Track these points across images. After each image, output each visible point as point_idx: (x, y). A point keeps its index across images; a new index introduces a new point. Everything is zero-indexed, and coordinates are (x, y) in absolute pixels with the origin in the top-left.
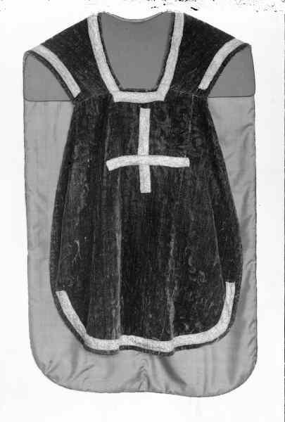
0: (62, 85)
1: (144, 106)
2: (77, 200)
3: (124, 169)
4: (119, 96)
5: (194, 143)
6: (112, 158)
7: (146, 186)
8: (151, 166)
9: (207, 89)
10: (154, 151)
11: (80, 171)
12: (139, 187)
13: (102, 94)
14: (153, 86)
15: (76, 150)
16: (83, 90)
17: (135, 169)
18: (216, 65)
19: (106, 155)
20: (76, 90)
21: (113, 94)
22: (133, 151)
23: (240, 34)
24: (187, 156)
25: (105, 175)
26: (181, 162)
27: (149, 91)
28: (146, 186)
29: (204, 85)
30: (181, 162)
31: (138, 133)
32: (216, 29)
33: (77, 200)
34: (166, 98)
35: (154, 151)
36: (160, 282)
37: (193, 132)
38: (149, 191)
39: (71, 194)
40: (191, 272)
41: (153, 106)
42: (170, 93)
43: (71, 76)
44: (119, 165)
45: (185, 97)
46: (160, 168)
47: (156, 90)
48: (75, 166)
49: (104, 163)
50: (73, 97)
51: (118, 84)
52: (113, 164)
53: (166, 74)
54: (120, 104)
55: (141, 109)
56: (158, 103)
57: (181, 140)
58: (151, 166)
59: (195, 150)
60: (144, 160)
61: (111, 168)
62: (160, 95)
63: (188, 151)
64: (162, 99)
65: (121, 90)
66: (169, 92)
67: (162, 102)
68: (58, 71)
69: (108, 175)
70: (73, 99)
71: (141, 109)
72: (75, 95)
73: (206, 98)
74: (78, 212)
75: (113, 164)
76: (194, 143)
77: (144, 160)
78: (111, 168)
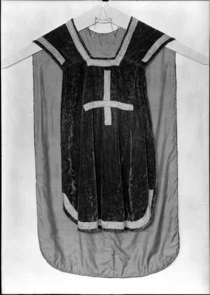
0: (67, 215)
1: (107, 68)
3: (94, 110)
4: (90, 63)
5: (136, 95)
6: (87, 102)
7: (108, 121)
8: (112, 108)
9: (147, 62)
12: (104, 121)
13: (79, 61)
14: (114, 56)
16: (67, 60)
17: (101, 110)
19: (83, 101)
20: (62, 60)
21: (86, 60)
22: (100, 98)
23: (168, 32)
25: (83, 114)
27: (110, 59)
28: (108, 121)
30: (128, 107)
31: (103, 86)
34: (120, 65)
36: (109, 196)
37: (136, 88)
42: (123, 61)
43: (57, 51)
44: (91, 107)
45: (132, 64)
47: (114, 58)
49: (82, 106)
50: (60, 64)
51: (89, 54)
52: (87, 107)
53: (122, 48)
54: (91, 67)
55: (105, 71)
56: (115, 67)
58: (112, 108)
60: (107, 104)
61: (86, 109)
62: (117, 62)
64: (118, 65)
65: (92, 58)
66: (123, 60)
67: (118, 66)
68: (49, 50)
69: (85, 115)
70: (61, 66)
71: (105, 71)
72: (62, 63)
73: (145, 68)
74: (69, 139)
75: (87, 107)
76: (136, 95)
77: (107, 104)
78: (86, 109)
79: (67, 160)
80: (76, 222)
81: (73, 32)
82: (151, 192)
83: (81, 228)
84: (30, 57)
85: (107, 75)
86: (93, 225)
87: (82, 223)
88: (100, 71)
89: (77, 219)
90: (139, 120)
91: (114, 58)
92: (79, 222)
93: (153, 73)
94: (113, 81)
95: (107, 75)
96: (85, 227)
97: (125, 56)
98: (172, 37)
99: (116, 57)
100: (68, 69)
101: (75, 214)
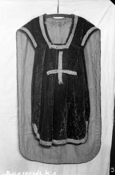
2: (39, 87)
7: (60, 80)
10: (64, 68)
11: (40, 76)
15: (37, 68)
18: (60, 78)
20: (36, 45)
23: (97, 25)
24: (76, 71)
26: (74, 73)
28: (60, 80)
29: (83, 44)
32: (88, 22)
33: (39, 87)
34: (69, 48)
35: (64, 68)
38: (76, 74)
39: (37, 86)
40: (76, 116)
41: (64, 50)
42: (71, 46)
46: (66, 74)
48: (37, 75)
52: (49, 73)
55: (60, 52)
56: (66, 49)
57: (74, 65)
59: (79, 69)
62: (67, 46)
63: (76, 69)
64: (68, 48)
65: (52, 44)
70: (35, 49)
71: (60, 52)
72: (88, 121)
75: (49, 73)
77: (60, 71)
79: (38, 104)
80: (38, 140)
81: (68, 43)
82: (87, 122)
83: (40, 143)
84: (44, 150)
85: (61, 53)
86: (49, 143)
87: (42, 141)
88: (57, 52)
89: (39, 138)
90: (46, 49)
91: (65, 44)
92: (40, 140)
93: (89, 51)
94: (63, 56)
95: (61, 53)
96: (43, 143)
97: (71, 42)
98: (98, 28)
99: (66, 43)
100: (38, 50)
101: (38, 136)
